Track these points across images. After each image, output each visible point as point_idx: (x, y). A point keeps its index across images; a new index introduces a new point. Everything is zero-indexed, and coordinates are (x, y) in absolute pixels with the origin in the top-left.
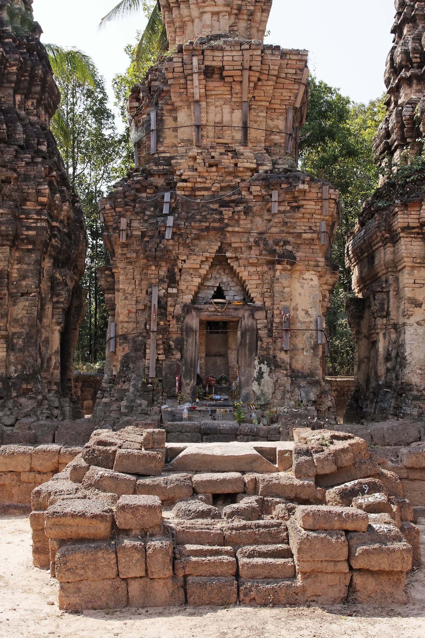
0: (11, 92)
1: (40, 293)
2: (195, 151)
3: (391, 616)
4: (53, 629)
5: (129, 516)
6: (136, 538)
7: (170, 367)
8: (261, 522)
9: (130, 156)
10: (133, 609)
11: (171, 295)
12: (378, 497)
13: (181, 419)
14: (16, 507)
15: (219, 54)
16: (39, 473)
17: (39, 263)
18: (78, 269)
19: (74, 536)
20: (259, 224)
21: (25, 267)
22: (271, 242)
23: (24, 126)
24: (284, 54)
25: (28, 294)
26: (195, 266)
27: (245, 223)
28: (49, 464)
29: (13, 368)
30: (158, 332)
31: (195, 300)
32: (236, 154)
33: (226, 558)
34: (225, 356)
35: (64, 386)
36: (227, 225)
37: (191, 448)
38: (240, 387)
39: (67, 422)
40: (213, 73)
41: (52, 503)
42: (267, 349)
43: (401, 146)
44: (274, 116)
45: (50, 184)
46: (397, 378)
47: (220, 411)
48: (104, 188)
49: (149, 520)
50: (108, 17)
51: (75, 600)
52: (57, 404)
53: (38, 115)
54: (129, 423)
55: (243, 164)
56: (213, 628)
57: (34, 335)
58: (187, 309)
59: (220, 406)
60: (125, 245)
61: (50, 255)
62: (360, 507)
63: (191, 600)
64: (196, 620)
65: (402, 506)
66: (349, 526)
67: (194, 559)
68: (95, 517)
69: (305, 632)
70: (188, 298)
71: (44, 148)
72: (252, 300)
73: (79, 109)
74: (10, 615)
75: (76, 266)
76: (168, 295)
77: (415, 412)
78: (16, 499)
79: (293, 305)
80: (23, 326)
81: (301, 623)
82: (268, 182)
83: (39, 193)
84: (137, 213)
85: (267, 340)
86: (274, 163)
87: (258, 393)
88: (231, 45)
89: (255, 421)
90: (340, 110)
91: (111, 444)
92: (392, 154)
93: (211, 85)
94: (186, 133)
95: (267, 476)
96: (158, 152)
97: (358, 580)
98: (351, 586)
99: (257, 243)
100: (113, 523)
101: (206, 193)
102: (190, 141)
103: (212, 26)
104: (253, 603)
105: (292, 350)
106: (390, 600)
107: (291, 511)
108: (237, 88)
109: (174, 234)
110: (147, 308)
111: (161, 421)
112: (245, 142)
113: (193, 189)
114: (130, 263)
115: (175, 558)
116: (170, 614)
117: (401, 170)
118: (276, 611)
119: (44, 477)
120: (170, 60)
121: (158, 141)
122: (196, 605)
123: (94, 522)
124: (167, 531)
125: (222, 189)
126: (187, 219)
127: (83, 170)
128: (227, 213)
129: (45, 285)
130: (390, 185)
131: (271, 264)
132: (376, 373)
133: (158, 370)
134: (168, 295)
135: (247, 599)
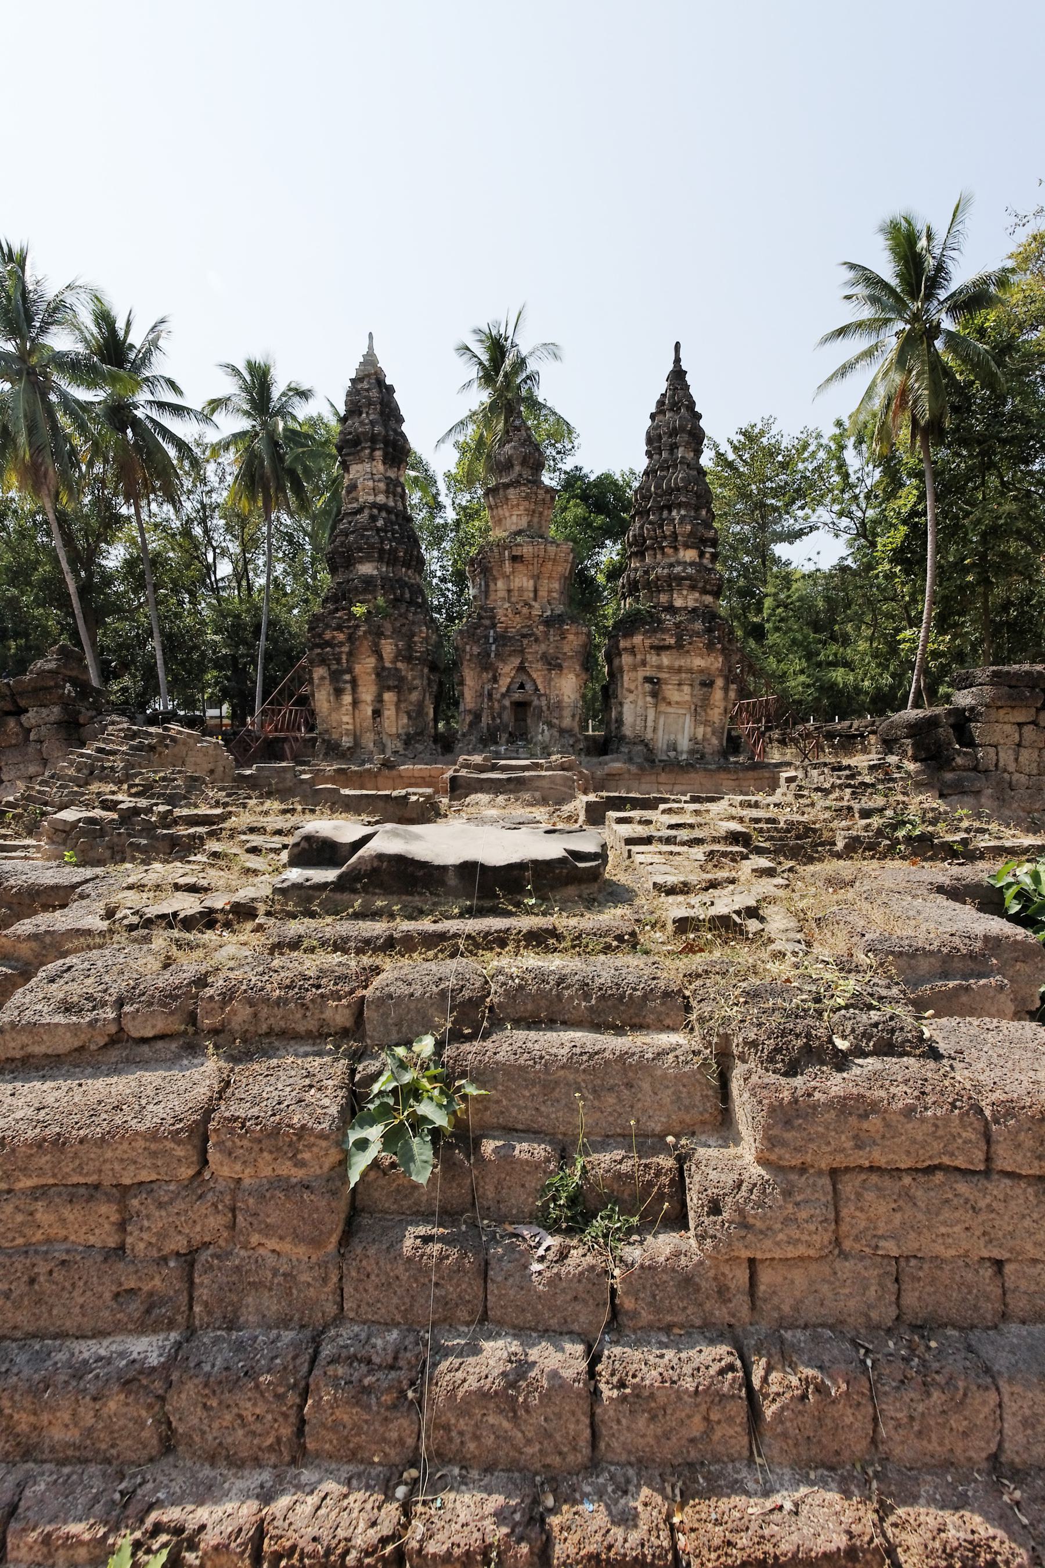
26: (507, 670)
27: (535, 647)
32: (531, 607)
37: (503, 762)
55: (535, 612)
57: (421, 705)
58: (503, 696)
70: (504, 690)
82: (548, 622)
85: (547, 713)
94: (502, 594)
110: (481, 695)
112: (535, 599)
128: (525, 642)
129: (425, 682)
131: (550, 670)
133: (488, 729)
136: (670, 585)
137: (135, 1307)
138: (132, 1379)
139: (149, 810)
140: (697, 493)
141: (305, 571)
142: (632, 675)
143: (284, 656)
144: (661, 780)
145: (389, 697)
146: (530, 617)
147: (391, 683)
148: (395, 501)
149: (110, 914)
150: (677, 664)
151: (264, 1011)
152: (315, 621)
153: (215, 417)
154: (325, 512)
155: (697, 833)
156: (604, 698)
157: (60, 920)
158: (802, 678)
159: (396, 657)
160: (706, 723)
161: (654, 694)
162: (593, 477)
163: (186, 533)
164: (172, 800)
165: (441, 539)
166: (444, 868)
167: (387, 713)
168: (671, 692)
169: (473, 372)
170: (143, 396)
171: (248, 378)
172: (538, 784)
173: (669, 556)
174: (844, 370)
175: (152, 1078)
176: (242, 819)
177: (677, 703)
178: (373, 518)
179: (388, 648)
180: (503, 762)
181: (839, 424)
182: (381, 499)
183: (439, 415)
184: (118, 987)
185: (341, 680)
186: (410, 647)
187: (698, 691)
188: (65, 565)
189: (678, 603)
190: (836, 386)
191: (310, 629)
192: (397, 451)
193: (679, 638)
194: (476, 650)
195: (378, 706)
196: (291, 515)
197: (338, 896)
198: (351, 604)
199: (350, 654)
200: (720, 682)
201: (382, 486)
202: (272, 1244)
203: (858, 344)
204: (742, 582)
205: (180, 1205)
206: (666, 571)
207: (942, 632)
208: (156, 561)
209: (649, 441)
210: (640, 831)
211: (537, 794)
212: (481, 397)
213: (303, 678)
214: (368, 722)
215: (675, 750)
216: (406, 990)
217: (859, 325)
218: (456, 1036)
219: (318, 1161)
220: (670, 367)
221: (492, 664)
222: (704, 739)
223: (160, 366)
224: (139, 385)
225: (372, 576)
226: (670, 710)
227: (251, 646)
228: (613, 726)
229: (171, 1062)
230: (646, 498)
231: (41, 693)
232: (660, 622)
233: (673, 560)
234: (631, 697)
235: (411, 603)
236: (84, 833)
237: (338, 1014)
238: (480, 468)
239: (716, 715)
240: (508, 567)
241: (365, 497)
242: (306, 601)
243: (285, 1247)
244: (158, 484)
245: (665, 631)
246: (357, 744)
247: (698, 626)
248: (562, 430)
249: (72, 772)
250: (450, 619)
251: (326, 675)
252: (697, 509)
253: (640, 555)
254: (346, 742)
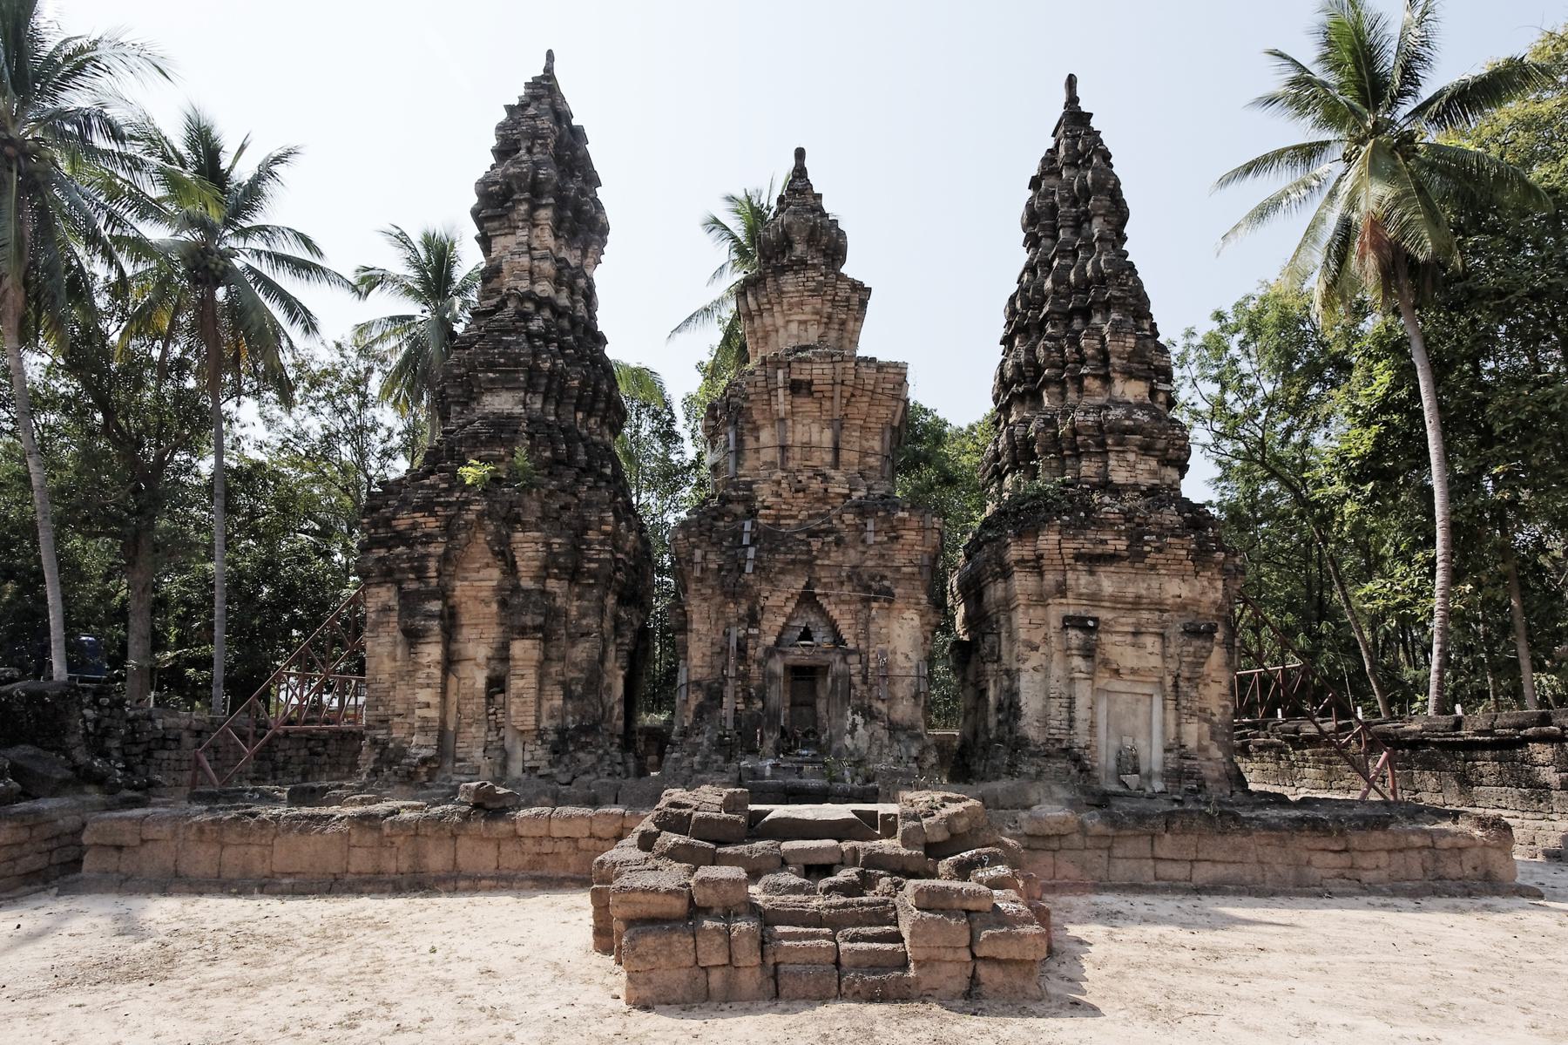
0: (572, 408)
1: (602, 634)
2: (779, 475)
3: (1023, 1016)
4: (620, 1029)
5: (709, 891)
6: (717, 918)
7: (750, 717)
8: (865, 899)
9: (701, 484)
10: (715, 1005)
11: (752, 636)
12: (1002, 870)
13: (763, 778)
14: (573, 880)
15: (808, 366)
16: (600, 839)
17: (601, 599)
18: (646, 608)
19: (644, 915)
20: (853, 556)
21: (585, 603)
22: (865, 577)
23: (586, 446)
24: (881, 367)
25: (588, 634)
26: (779, 601)
27: (836, 556)
28: (612, 828)
29: (570, 719)
30: (737, 678)
31: (777, 644)
32: (826, 478)
33: (825, 943)
34: (812, 705)
35: (628, 740)
36: (816, 558)
37: (779, 811)
38: (830, 740)
39: (630, 780)
40: (800, 388)
41: (618, 876)
42: (861, 698)
43: (1012, 470)
44: (869, 436)
45: (615, 512)
46: (1011, 731)
47: (807, 768)
48: (671, 518)
49: (733, 896)
50: (678, 329)
51: (645, 992)
52: (619, 759)
53: (601, 435)
54: (704, 782)
55: (835, 489)
56: (812, 1028)
57: (594, 678)
58: (770, 652)
59: (807, 762)
60: (700, 580)
61: (614, 592)
62: (980, 882)
63: (783, 992)
64: (790, 1018)
65: (1028, 879)
66: (971, 905)
67: (786, 943)
68: (669, 892)
69: (923, 1035)
70: (770, 640)
71: (608, 471)
72: (844, 643)
73: (645, 431)
74: (568, 1011)
75: (642, 604)
76: (747, 636)
77: (1033, 770)
78: (572, 869)
79: (891, 647)
80: (582, 671)
81: (918, 1023)
82: (862, 510)
83: (602, 521)
84: (714, 544)
85: (861, 687)
86: (869, 488)
87: (851, 747)
88: (821, 356)
89: (849, 780)
90: (937, 433)
91: (686, 806)
92: (1002, 478)
93: (798, 401)
94: (768, 455)
95: (868, 844)
96: (737, 476)
97: (983, 971)
98: (974, 979)
99: (850, 578)
100: (691, 899)
101: (792, 522)
102: (773, 464)
103: (799, 337)
104: (858, 997)
105: (890, 699)
106: (1021, 996)
107: (898, 886)
108: (827, 404)
109: (755, 567)
110: (724, 650)
111: (740, 779)
112: (836, 464)
113: (778, 517)
114: (705, 600)
115: (764, 943)
116: (759, 1011)
117: (1014, 496)
118: (884, 1007)
119: (606, 844)
120: (752, 373)
121: (737, 464)
122: (792, 999)
123: (669, 898)
124: (753, 910)
125: (810, 517)
126: (770, 551)
127: (647, 499)
128: (816, 544)
129: (608, 625)
130: (1000, 514)
131: (866, 602)
132: (986, 725)
133: (737, 721)
134: (747, 636)
135: (850, 992)
136: (1102, 444)
144: (1160, 853)
145: (523, 650)
146: (824, 497)
147: (528, 620)
148: (574, 302)
150: (1131, 591)
156: (972, 656)
159: (545, 567)
161: (1088, 652)
167: (516, 684)
171: (423, 254)
173: (1092, 394)
174: (1262, 212)
177: (1134, 671)
179: (528, 549)
180: (779, 811)
181: (1219, 316)
182: (544, 288)
186: (577, 546)
189: (1119, 476)
193: (1136, 538)
195: (500, 668)
199: (445, 559)
201: (547, 267)
206: (1091, 418)
209: (1033, 217)
214: (476, 706)
215: (1136, 771)
220: (1059, 110)
221: (747, 586)
222: (1202, 749)
223: (275, 210)
225: (510, 416)
226: (1117, 685)
232: (1090, 510)
233: (1100, 400)
234: (1035, 659)
240: (782, 402)
245: (1102, 525)
251: (394, 603)
254: (421, 746)
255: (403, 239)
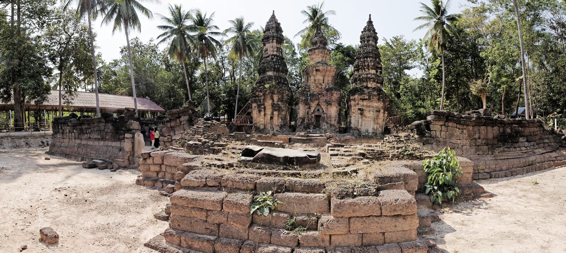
20: (326, 98)
26: (314, 105)
27: (323, 98)
32: (322, 85)
57: (285, 116)
58: (312, 113)
82: (327, 90)
137: (209, 231)
138: (208, 241)
139: (208, 142)
140: (376, 54)
141: (251, 73)
142: (354, 107)
143: (244, 100)
145: (276, 113)
147: (276, 108)
149: (202, 163)
150: (368, 105)
151: (235, 184)
152: (254, 89)
153: (227, 34)
154: (258, 56)
155: (351, 153)
156: (344, 115)
157: (192, 164)
158: (411, 111)
160: (377, 124)
161: (361, 114)
162: (345, 46)
163: (217, 65)
164: (214, 140)
165: (296, 63)
166: (280, 158)
168: (366, 113)
169: (307, 17)
170: (208, 31)
172: (316, 140)
174: (421, 27)
175: (212, 193)
176: (231, 145)
178: (272, 59)
179: (276, 98)
182: (275, 53)
183: (295, 30)
184: (206, 176)
185: (261, 107)
186: (283, 98)
187: (376, 114)
188: (186, 77)
189: (369, 86)
190: (418, 31)
191: (252, 92)
192: (280, 39)
193: (369, 96)
194: (304, 98)
196: (248, 58)
197: (253, 163)
198: (265, 84)
199: (264, 99)
200: (382, 111)
201: (276, 49)
202: (235, 224)
203: (425, 22)
204: (394, 80)
205: (217, 215)
207: (447, 100)
208: (209, 73)
209: (361, 38)
210: (336, 152)
211: (316, 144)
212: (309, 24)
213: (250, 107)
216: (266, 181)
217: (424, 18)
218: (277, 192)
219: (244, 211)
223: (212, 24)
224: (207, 29)
227: (234, 97)
228: (348, 124)
229: (216, 191)
230: (360, 54)
231: (184, 112)
232: (363, 91)
234: (354, 115)
235: (283, 84)
236: (194, 147)
237: (251, 186)
238: (308, 42)
239: (380, 121)
240: (314, 73)
241: (270, 53)
242: (251, 83)
243: (238, 225)
244: (210, 53)
245: (365, 94)
246: (265, 128)
247: (375, 93)
248: (335, 33)
249: (191, 132)
250: (298, 88)
252: (376, 58)
253: (358, 70)
254: (262, 127)
255: (233, 22)
